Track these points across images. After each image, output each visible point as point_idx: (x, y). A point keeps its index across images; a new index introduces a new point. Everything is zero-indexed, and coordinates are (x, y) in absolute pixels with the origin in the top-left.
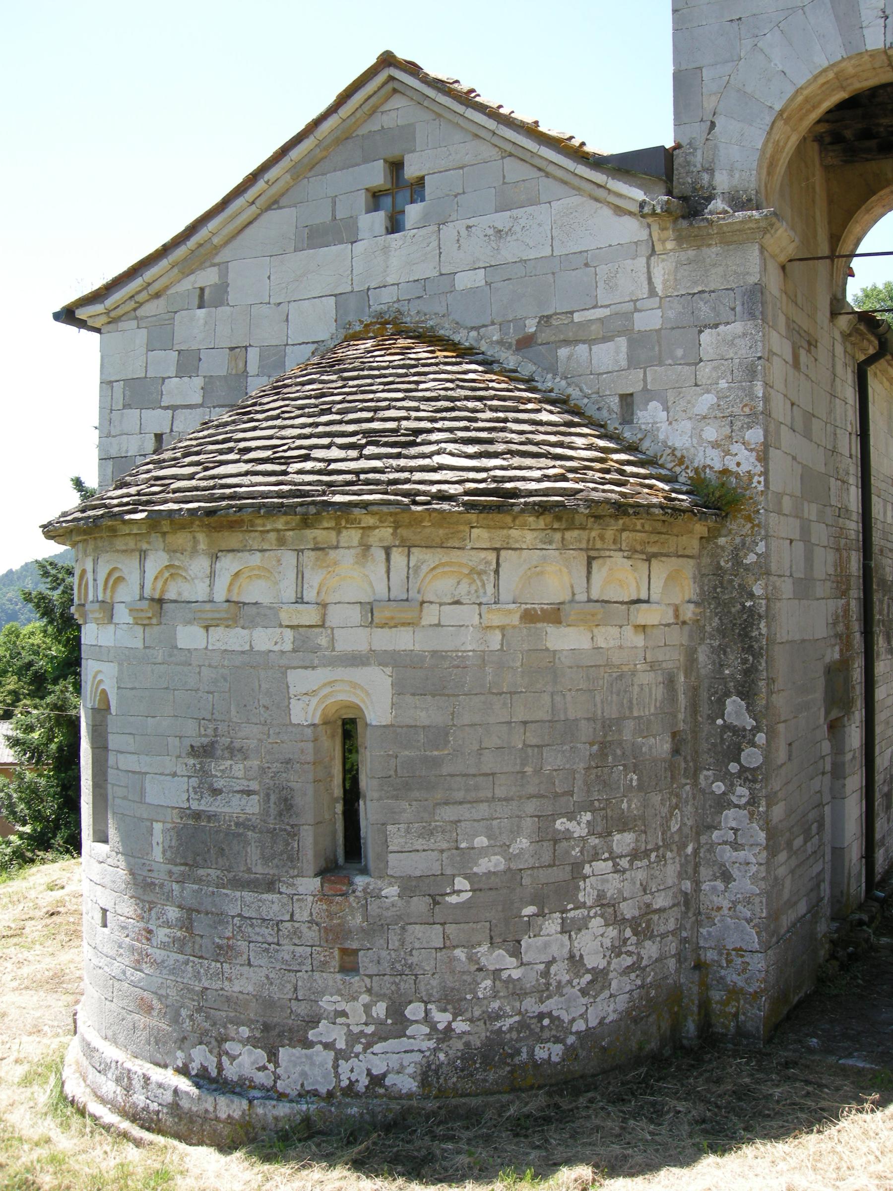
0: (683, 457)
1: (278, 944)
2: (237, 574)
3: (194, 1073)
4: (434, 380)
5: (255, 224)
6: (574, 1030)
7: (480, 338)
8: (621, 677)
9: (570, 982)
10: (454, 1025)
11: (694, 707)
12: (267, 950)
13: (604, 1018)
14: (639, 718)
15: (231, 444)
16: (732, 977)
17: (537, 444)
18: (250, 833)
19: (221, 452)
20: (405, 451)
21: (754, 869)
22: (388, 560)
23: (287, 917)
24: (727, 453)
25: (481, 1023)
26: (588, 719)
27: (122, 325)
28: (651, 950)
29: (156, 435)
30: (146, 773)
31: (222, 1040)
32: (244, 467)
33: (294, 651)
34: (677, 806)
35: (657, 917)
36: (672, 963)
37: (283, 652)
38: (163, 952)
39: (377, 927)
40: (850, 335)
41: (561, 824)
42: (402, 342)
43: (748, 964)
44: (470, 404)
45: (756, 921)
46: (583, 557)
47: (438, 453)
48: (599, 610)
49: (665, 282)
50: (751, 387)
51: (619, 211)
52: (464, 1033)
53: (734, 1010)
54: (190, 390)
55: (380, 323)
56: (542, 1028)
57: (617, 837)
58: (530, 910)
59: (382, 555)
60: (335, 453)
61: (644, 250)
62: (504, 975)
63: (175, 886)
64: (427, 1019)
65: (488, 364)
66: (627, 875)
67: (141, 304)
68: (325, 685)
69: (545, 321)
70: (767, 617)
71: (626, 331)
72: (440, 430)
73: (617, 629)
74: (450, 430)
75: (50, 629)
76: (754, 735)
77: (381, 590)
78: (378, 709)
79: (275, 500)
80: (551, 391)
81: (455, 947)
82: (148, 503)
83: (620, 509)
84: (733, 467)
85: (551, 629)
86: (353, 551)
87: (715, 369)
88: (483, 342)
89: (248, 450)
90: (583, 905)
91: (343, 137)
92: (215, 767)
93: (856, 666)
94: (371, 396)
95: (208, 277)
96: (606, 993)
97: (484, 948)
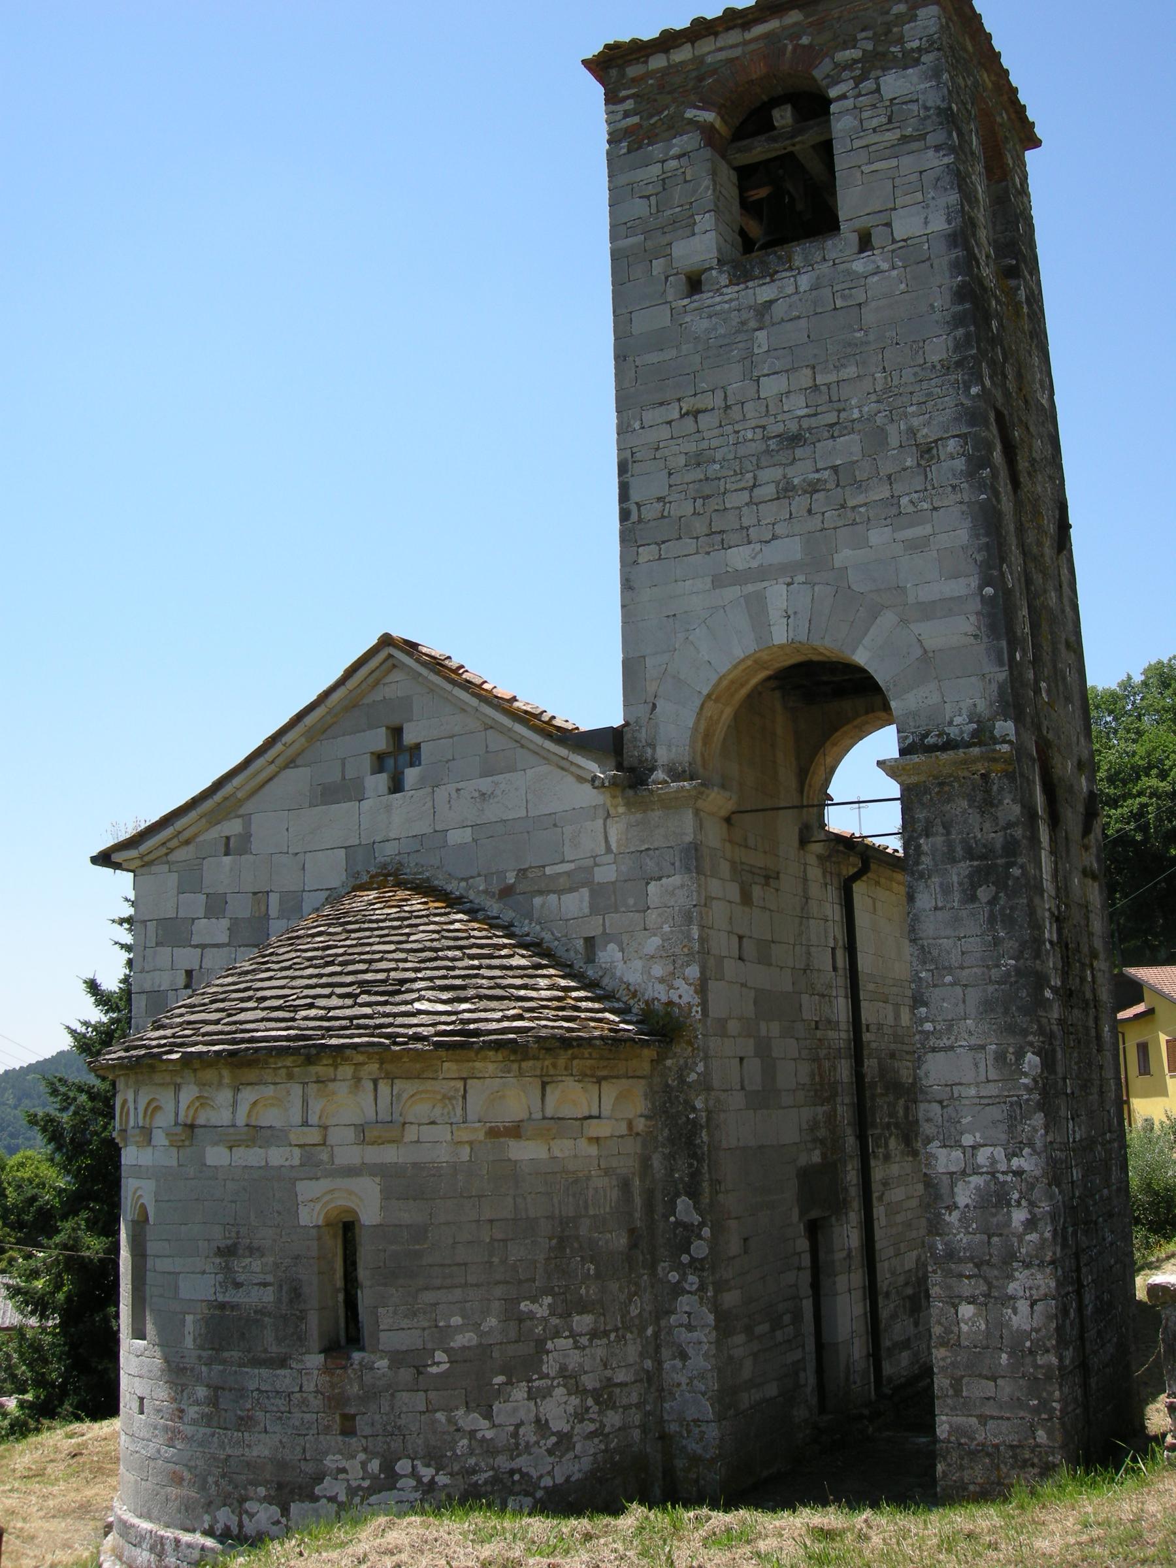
0: (636, 991)
1: (289, 1412)
2: (255, 1104)
3: (218, 1533)
4: (423, 932)
5: (275, 780)
6: (542, 1485)
7: (469, 888)
8: (576, 1181)
9: (537, 1443)
10: (437, 1479)
11: (649, 1206)
12: (280, 1418)
13: (570, 1476)
14: (595, 1216)
15: (251, 993)
16: (693, 1446)
17: (504, 988)
18: (266, 1319)
19: (242, 1000)
20: (391, 999)
21: (706, 1347)
22: (376, 1089)
23: (297, 1389)
24: (671, 987)
25: (460, 1477)
26: (547, 1217)
27: (154, 869)
28: (613, 1419)
29: (186, 971)
30: (179, 1273)
31: (243, 1500)
32: (260, 1014)
33: (301, 1165)
34: (636, 1294)
35: (618, 1390)
36: (636, 1434)
37: (292, 1167)
38: (193, 1428)
39: (370, 1395)
40: (829, 856)
41: (525, 1306)
42: (401, 894)
43: (704, 1432)
44: (450, 954)
45: (710, 1394)
46: (537, 1083)
47: (418, 999)
48: (555, 1126)
49: (618, 841)
50: (689, 931)
51: (581, 779)
52: (445, 1485)
53: (695, 1476)
54: (218, 930)
55: (383, 875)
56: (513, 1482)
57: (577, 1318)
58: (500, 1379)
59: (371, 1085)
60: (335, 1001)
61: (601, 813)
62: (479, 1435)
63: (204, 1368)
64: (414, 1474)
65: (473, 913)
66: (587, 1351)
67: (172, 850)
68: (326, 1193)
69: (522, 873)
70: (708, 1126)
71: (588, 883)
72: (422, 979)
73: (572, 1142)
74: (431, 979)
75: (58, 1157)
76: (701, 1230)
77: (370, 1114)
78: (370, 1215)
79: (284, 1043)
80: (527, 935)
81: (436, 1411)
82: (182, 1045)
83: (566, 1042)
84: (676, 999)
85: (512, 1143)
86: (347, 1083)
87: (660, 915)
88: (471, 892)
89: (264, 999)
90: (547, 1376)
91: (352, 705)
92: (237, 1265)
93: (849, 1167)
94: (368, 949)
95: (233, 827)
96: (571, 1455)
97: (460, 1412)
